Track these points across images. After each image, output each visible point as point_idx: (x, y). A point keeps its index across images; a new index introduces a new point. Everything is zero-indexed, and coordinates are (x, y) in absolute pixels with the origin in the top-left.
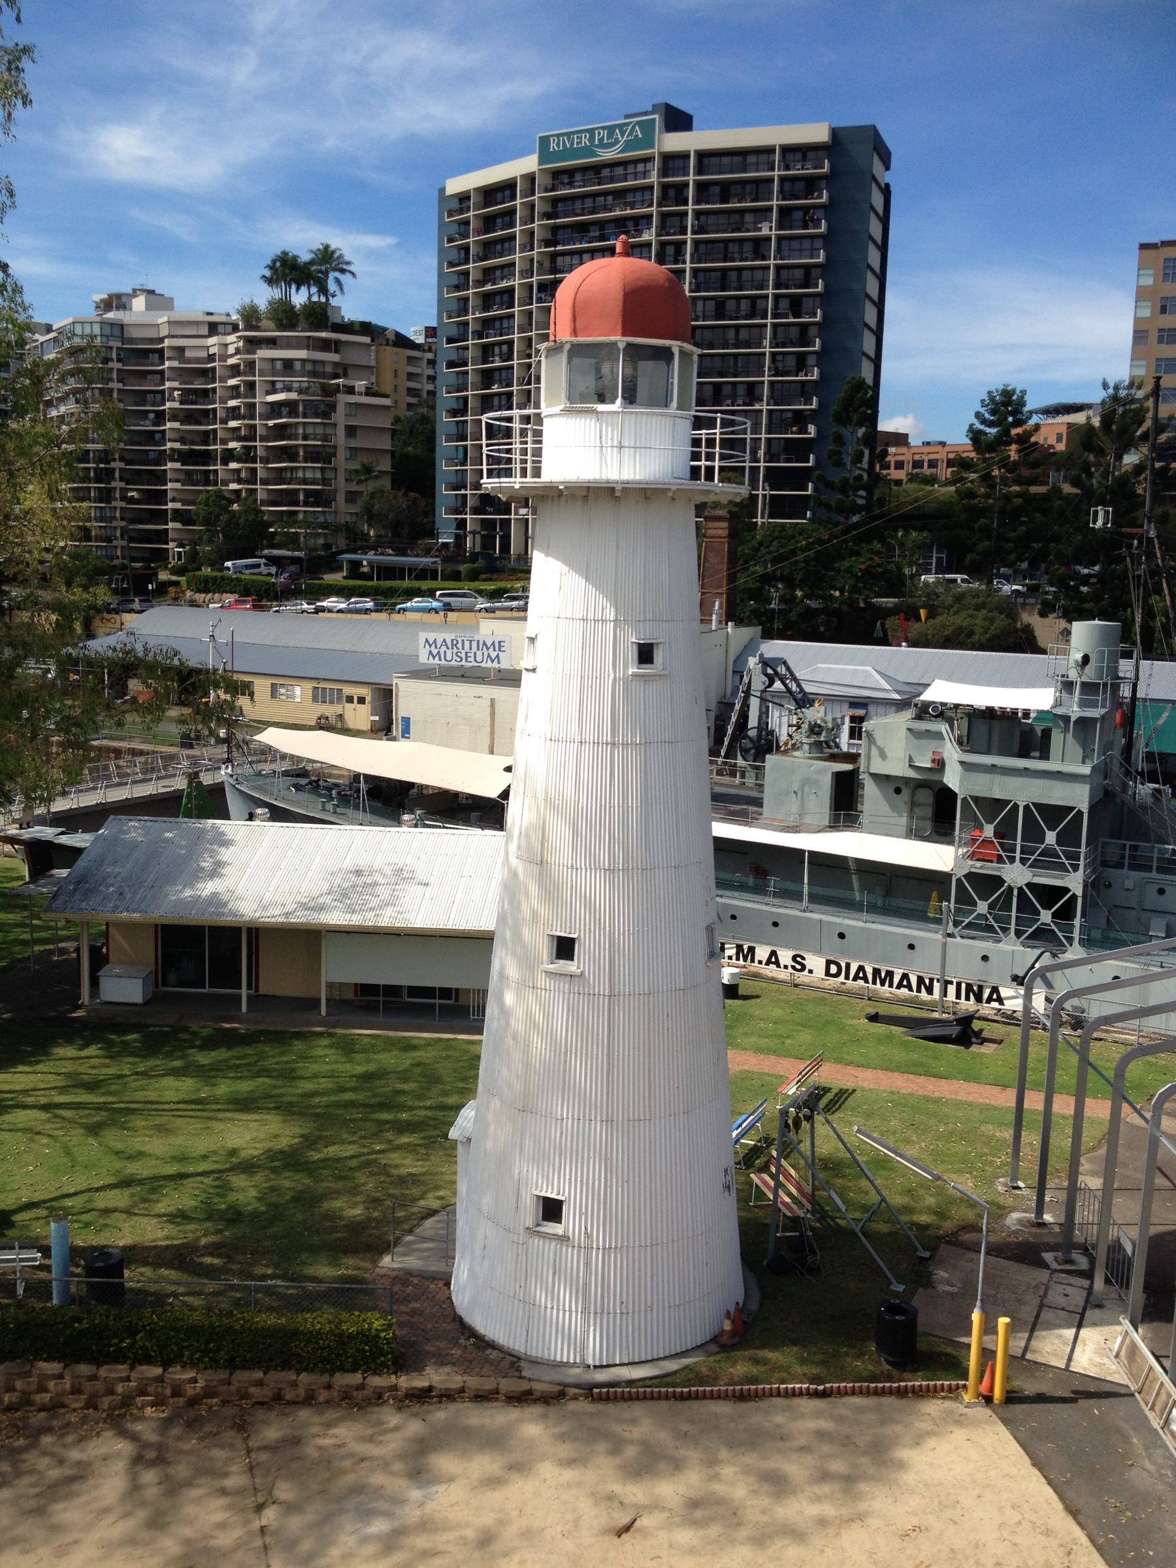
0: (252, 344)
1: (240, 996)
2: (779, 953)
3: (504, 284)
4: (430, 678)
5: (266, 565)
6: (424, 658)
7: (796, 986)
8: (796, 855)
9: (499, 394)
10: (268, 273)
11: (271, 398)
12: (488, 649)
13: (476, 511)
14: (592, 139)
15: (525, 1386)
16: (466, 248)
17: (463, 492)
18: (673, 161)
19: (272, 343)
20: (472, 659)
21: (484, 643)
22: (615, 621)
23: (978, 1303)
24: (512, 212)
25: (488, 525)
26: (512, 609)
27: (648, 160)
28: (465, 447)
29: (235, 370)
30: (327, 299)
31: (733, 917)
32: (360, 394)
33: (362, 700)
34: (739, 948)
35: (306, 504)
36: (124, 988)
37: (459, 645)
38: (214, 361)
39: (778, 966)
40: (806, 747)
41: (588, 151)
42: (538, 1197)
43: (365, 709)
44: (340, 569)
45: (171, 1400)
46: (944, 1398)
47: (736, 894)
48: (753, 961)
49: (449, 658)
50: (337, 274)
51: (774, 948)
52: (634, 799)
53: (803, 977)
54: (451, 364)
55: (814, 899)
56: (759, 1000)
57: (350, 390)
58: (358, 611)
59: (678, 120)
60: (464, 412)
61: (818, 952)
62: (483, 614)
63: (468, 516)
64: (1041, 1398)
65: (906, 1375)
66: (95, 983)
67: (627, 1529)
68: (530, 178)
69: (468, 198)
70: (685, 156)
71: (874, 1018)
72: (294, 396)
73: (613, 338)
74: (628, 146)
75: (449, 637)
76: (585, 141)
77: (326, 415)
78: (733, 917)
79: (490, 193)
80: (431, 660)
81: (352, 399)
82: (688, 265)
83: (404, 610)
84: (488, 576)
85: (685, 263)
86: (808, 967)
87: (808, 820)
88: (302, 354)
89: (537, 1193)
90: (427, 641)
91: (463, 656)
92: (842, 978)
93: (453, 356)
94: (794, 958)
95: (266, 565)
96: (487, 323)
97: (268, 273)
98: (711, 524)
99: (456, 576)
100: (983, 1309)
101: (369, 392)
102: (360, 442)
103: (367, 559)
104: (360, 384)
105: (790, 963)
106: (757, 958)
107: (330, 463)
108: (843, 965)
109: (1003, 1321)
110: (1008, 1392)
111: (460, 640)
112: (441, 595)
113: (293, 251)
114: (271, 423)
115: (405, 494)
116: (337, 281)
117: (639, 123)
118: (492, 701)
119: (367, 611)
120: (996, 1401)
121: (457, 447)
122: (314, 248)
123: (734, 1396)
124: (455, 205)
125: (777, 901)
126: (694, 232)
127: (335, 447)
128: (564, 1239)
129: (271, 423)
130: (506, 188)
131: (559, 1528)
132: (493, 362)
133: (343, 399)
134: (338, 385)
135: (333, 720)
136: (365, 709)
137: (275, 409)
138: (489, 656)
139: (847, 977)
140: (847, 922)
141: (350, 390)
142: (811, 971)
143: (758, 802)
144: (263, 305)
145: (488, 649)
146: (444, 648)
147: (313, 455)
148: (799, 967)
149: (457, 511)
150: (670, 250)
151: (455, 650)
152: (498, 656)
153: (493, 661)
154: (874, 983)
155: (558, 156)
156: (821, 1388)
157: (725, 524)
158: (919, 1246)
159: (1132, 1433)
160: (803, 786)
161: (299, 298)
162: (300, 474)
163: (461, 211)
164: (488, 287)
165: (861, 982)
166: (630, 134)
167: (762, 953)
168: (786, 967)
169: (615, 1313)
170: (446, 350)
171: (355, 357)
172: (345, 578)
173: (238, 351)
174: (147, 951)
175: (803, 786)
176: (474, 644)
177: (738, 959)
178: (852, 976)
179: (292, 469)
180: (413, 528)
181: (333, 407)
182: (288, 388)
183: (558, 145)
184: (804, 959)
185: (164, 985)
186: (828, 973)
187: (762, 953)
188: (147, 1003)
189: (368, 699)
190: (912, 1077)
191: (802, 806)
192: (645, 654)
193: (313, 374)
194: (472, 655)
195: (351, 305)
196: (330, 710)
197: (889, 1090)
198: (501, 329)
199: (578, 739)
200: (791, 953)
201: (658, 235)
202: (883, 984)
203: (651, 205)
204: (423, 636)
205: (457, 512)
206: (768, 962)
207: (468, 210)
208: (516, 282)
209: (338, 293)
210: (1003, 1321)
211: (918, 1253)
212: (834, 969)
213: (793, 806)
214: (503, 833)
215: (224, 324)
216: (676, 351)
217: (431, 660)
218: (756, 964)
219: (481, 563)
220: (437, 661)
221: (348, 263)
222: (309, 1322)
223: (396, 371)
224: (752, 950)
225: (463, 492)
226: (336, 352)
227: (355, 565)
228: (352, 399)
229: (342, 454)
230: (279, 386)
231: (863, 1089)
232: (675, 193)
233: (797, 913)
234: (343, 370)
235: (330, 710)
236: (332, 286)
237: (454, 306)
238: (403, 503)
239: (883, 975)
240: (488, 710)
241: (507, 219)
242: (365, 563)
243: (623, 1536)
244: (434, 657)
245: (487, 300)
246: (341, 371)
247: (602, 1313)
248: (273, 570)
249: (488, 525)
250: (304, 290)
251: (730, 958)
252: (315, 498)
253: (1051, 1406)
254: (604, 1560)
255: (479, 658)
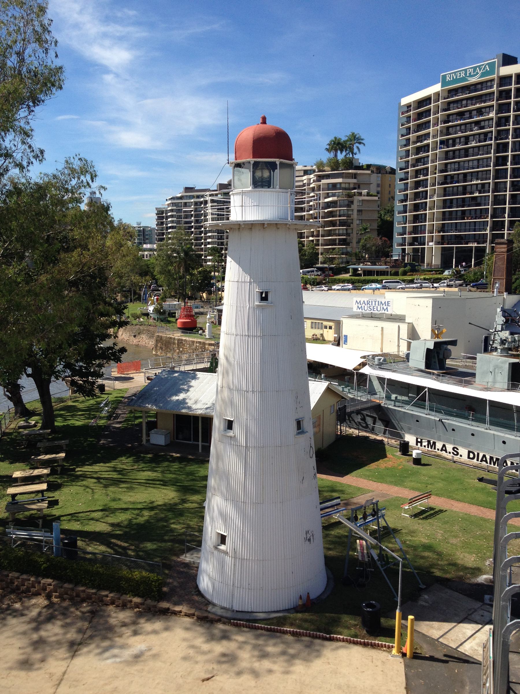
0: (320, 178)
1: (198, 445)
2: (437, 444)
3: (426, 142)
4: (357, 318)
5: (316, 271)
6: (355, 309)
7: (455, 462)
8: (483, 401)
9: (422, 192)
10: (328, 147)
11: (327, 200)
12: (383, 305)
13: (410, 244)
14: (466, 74)
15: (205, 614)
16: (409, 128)
17: (405, 236)
18: (505, 80)
19: (328, 177)
20: (375, 310)
21: (381, 302)
22: (250, 282)
23: (398, 607)
24: (429, 110)
25: (415, 251)
26: (414, 288)
27: (492, 80)
28: (406, 216)
29: (313, 190)
30: (353, 156)
31: (453, 430)
32: (364, 196)
33: (330, 328)
34: (429, 442)
35: (339, 244)
36: (158, 439)
37: (370, 303)
38: (305, 186)
39: (446, 452)
40: (499, 350)
41: (464, 79)
42: (219, 533)
43: (332, 332)
44: (349, 272)
45: (76, 598)
46: (384, 651)
47: (455, 419)
48: (435, 449)
49: (366, 309)
50: (357, 145)
51: (444, 443)
52: (257, 361)
53: (456, 458)
54: (401, 180)
55: (492, 423)
56: (429, 467)
57: (360, 194)
58: (345, 290)
59: (508, 60)
60: (406, 200)
61: (464, 446)
62: (400, 290)
63: (406, 247)
64: (432, 659)
65: (371, 638)
66: (148, 435)
67: (208, 679)
68: (437, 94)
69: (411, 106)
70: (510, 77)
71: (481, 480)
72: (335, 198)
73: (248, 160)
74: (483, 75)
75: (366, 300)
76: (463, 75)
77: (348, 206)
78: (453, 430)
79: (421, 103)
80: (358, 310)
81: (361, 198)
82: (511, 127)
83: (365, 289)
84: (411, 273)
85: (509, 125)
86: (460, 454)
87: (498, 385)
88: (340, 180)
89: (219, 532)
90: (357, 301)
91: (372, 308)
92: (475, 460)
93: (403, 176)
94: (453, 449)
95: (316, 271)
96: (418, 160)
97: (328, 147)
98: (498, 246)
99: (396, 274)
100: (401, 610)
101: (368, 195)
102: (365, 217)
103: (360, 267)
104: (364, 192)
105: (452, 451)
106: (437, 448)
107: (350, 226)
108: (476, 454)
109: (411, 617)
110: (414, 653)
111: (371, 301)
112: (385, 282)
113: (339, 136)
114: (326, 211)
115: (381, 239)
116: (358, 148)
117: (488, 64)
118: (382, 328)
119: (349, 290)
120: (408, 656)
121: (403, 216)
122: (348, 135)
123: (290, 633)
124: (406, 109)
125: (473, 423)
126: (514, 111)
127: (353, 219)
128: (226, 553)
129: (326, 211)
130: (426, 101)
131: (181, 673)
132: (420, 177)
133: (356, 198)
134: (355, 192)
135: (319, 336)
136: (332, 332)
137: (328, 205)
138: (358, 307)
139: (478, 460)
140: (507, 436)
141: (360, 194)
142: (461, 456)
143: (473, 375)
144: (325, 160)
145: (383, 305)
146: (364, 305)
147: (342, 223)
148: (455, 453)
149: (402, 245)
150: (503, 121)
151: (369, 305)
152: (387, 308)
153: (385, 310)
154: (490, 464)
155: (450, 83)
156: (362, 641)
157: (506, 246)
158: (420, 582)
159: (468, 684)
160: (495, 369)
161: (341, 156)
162: (337, 232)
163: (407, 112)
164: (419, 144)
165: (484, 463)
166: (484, 69)
167: (439, 445)
168: (450, 453)
169: (246, 589)
170: (400, 174)
171: (361, 179)
172: (350, 276)
173: (314, 181)
174: (170, 424)
175: (495, 369)
176: (377, 303)
177: (428, 447)
178: (480, 459)
179: (334, 230)
180: (383, 253)
181: (352, 202)
182: (334, 195)
183: (450, 78)
184: (458, 449)
185: (177, 439)
186: (469, 457)
187: (439, 445)
188: (166, 446)
189: (333, 327)
190: (482, 508)
191: (494, 378)
192: (264, 297)
193: (345, 189)
194: (376, 308)
195: (364, 158)
196: (318, 332)
197: (465, 512)
198: (424, 162)
199: (235, 333)
200: (452, 446)
201: (497, 114)
202: (494, 464)
203: (494, 101)
204: (355, 299)
205: (402, 245)
206: (442, 450)
207: (411, 111)
208: (430, 141)
209: (358, 152)
210: (411, 617)
211: (420, 586)
212: (471, 455)
213: (490, 378)
214: (216, 374)
215: (310, 170)
216: (278, 163)
217: (358, 310)
218: (436, 450)
219: (408, 267)
220: (361, 310)
221: (362, 139)
222: (143, 575)
223: (390, 185)
224: (434, 443)
225: (405, 236)
226: (355, 178)
227: (355, 270)
228: (361, 198)
229: (356, 222)
230: (330, 194)
231: (452, 511)
232: (506, 94)
233: (483, 430)
234: (358, 186)
235: (318, 332)
236: (356, 150)
237: (404, 154)
238: (380, 242)
239: (495, 460)
240: (380, 332)
241: (428, 113)
242: (360, 269)
243: (205, 682)
244: (359, 309)
245: (418, 150)
246: (357, 187)
247: (240, 587)
248: (319, 273)
249: (415, 251)
250: (344, 153)
251: (425, 446)
252: (343, 242)
253: (435, 664)
254: (190, 690)
255: (379, 309)
